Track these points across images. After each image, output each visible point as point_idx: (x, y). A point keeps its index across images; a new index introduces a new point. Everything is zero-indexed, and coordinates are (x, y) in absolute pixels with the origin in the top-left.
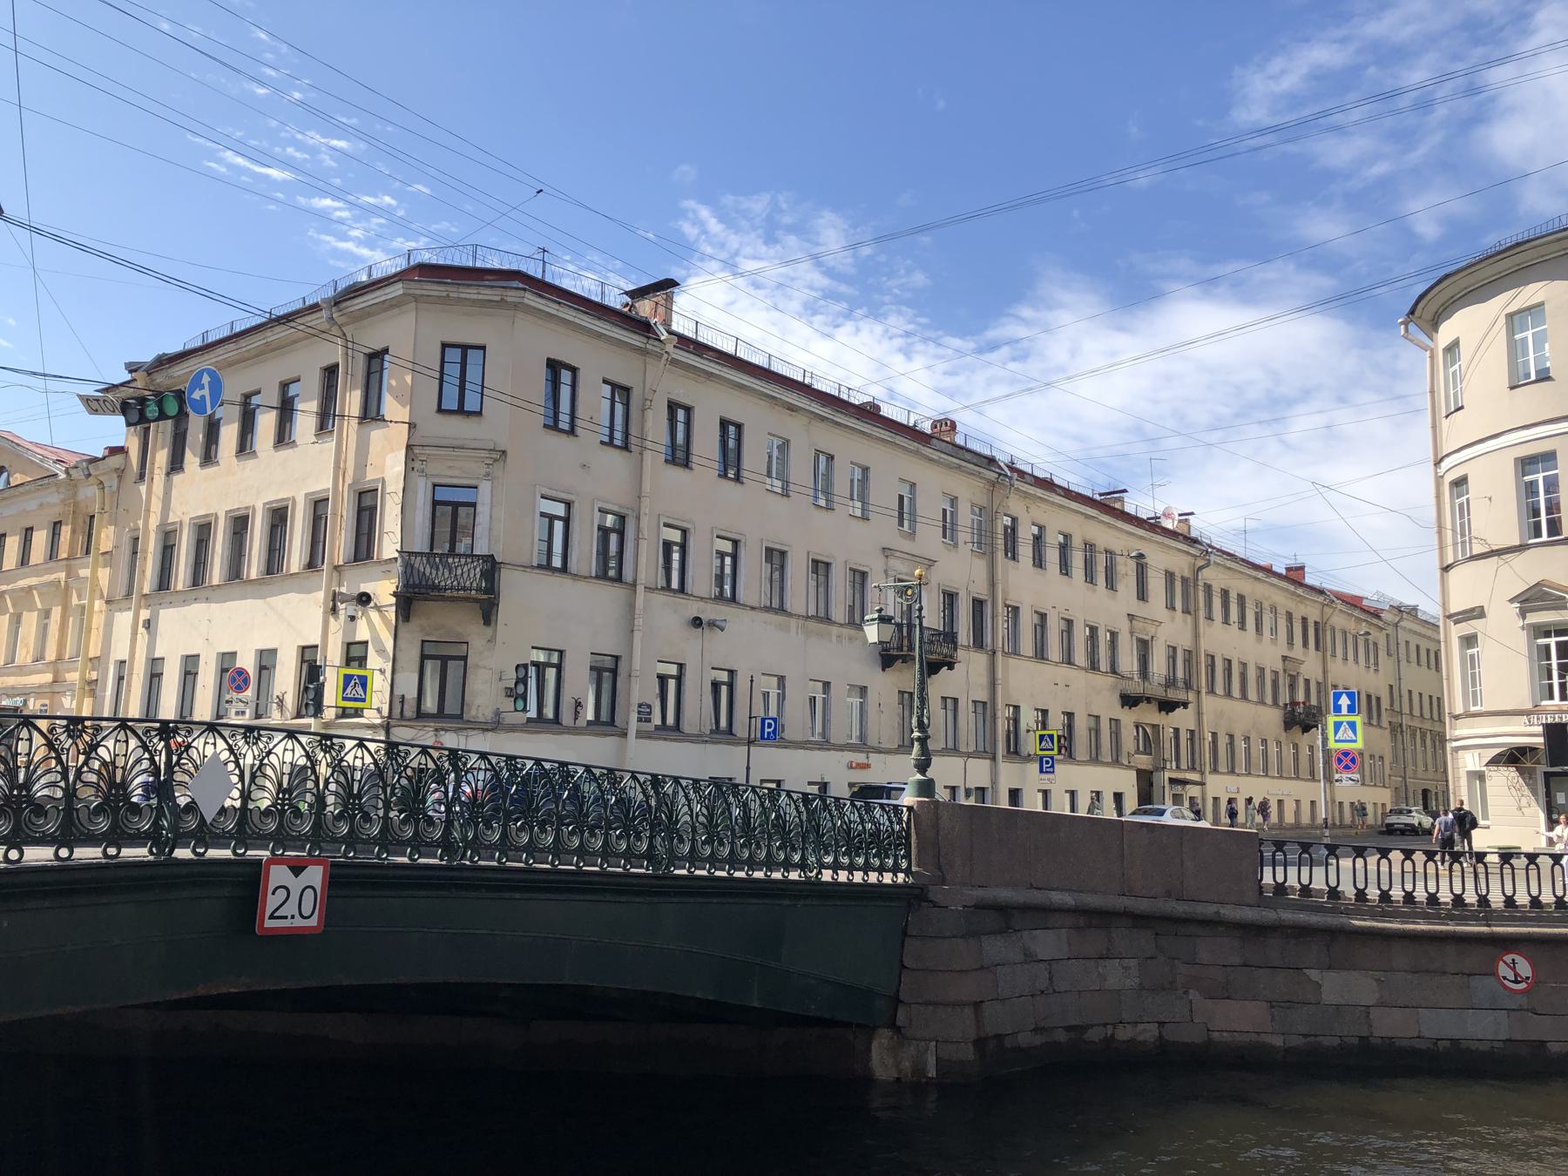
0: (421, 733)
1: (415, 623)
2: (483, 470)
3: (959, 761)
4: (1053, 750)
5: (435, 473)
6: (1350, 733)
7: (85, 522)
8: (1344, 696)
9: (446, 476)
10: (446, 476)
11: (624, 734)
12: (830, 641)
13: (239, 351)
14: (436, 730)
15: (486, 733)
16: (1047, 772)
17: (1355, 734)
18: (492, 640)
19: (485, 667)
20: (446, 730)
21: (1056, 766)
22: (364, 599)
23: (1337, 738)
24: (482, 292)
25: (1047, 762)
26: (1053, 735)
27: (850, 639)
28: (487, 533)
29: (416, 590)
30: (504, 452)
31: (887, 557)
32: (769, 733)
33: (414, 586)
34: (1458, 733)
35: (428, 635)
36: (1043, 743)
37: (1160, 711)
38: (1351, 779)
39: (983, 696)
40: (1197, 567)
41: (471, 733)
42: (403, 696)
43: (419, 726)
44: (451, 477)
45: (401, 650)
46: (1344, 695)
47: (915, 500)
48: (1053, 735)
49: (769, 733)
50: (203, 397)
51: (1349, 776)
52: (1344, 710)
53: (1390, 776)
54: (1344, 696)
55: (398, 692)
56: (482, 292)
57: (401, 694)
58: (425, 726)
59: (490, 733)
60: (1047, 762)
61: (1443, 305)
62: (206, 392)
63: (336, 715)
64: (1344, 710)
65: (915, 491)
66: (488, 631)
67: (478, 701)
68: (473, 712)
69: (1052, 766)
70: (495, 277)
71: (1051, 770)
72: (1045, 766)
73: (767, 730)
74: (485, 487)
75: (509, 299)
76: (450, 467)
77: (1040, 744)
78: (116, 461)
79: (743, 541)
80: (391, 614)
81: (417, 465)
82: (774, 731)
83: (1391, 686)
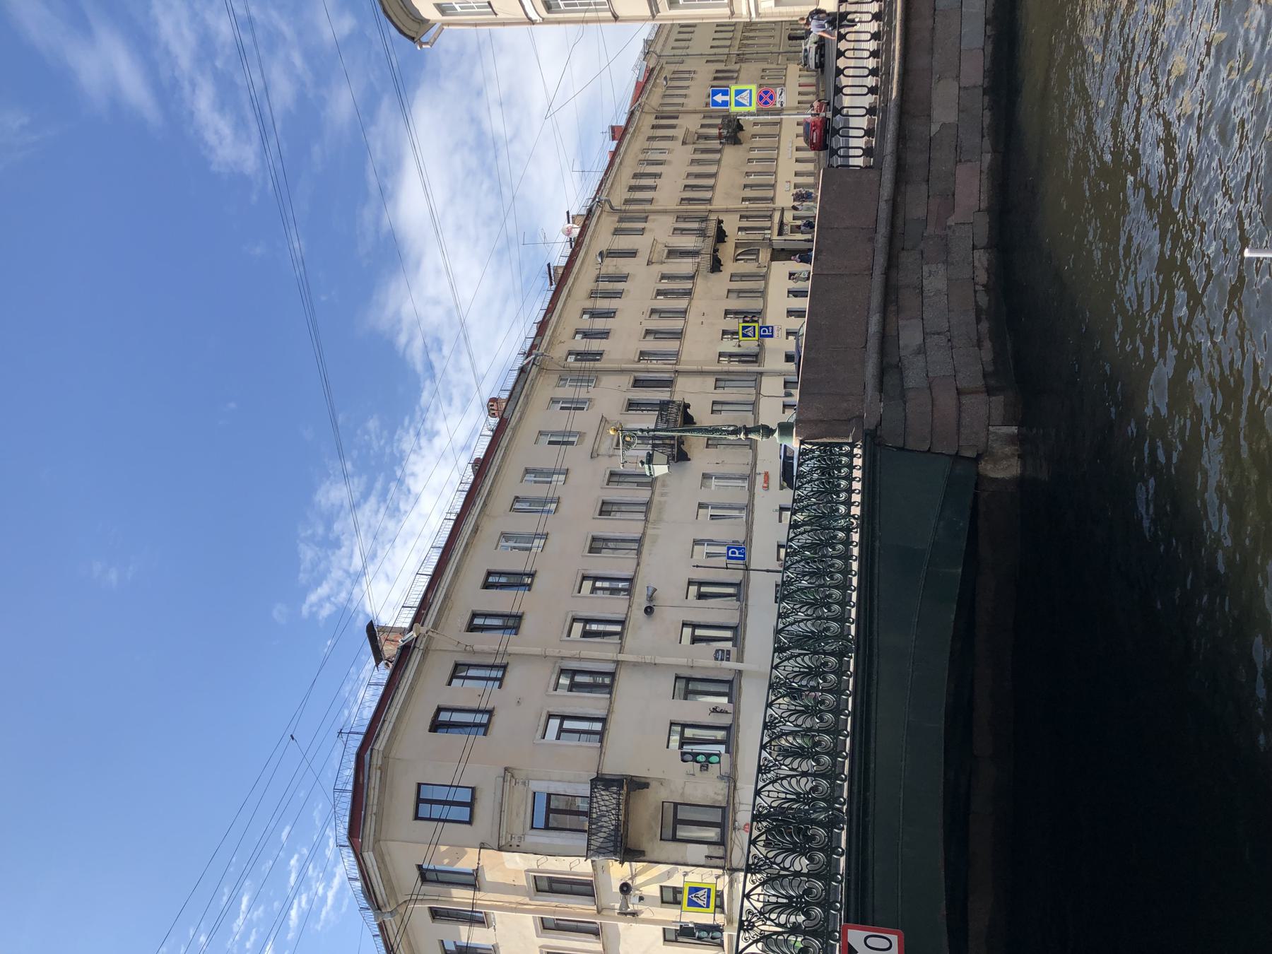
0: (737, 842)
1: (646, 846)
2: (520, 787)
4: (754, 327)
17: (746, 90)
18: (661, 782)
19: (683, 788)
20: (735, 821)
22: (625, 888)
24: (373, 786)
30: (506, 769)
31: (598, 455)
32: (740, 554)
34: (745, 12)
36: (749, 334)
38: (781, 95)
41: (737, 800)
42: (706, 857)
49: (740, 554)
52: (726, 98)
56: (373, 786)
58: (731, 839)
64: (726, 98)
65: (545, 432)
66: (653, 784)
67: (712, 794)
68: (720, 798)
69: (768, 327)
71: (770, 328)
72: (767, 333)
73: (737, 555)
74: (535, 786)
79: (583, 572)
81: (515, 842)
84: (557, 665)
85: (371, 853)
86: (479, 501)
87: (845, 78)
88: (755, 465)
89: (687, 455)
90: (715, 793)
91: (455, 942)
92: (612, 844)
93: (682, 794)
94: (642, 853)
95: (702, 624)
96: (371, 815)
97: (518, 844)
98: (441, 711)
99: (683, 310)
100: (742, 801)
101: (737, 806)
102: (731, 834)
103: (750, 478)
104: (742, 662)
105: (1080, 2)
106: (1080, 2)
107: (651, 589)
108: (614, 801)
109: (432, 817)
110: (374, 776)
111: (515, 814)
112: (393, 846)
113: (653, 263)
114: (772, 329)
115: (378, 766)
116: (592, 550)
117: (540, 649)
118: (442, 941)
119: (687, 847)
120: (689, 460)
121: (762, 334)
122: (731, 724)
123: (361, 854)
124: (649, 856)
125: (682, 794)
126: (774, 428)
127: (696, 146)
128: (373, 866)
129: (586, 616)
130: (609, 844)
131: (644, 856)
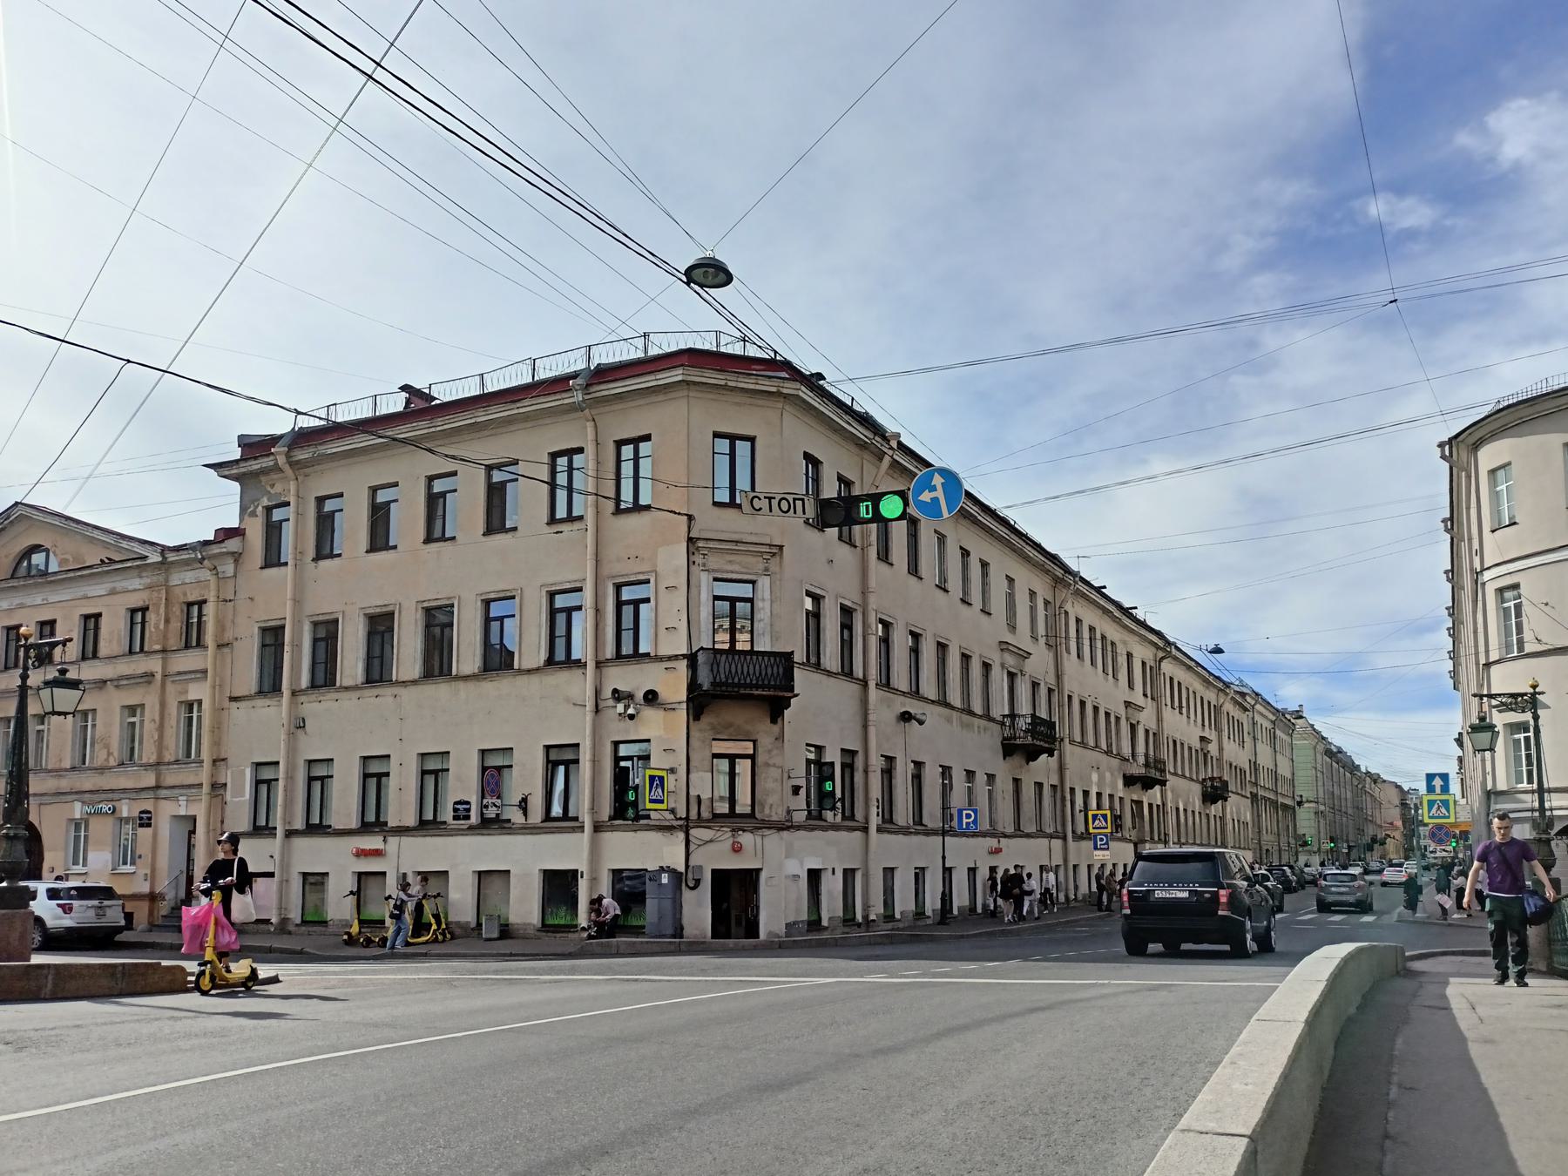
0: (720, 833)
1: (706, 720)
2: (761, 566)
3: (1045, 841)
4: (1107, 828)
5: (716, 567)
6: (1443, 810)
7: (182, 611)
8: (1437, 778)
9: (727, 572)
10: (727, 572)
11: (865, 829)
12: (974, 732)
13: (433, 430)
14: (733, 830)
15: (781, 832)
16: (1101, 849)
17: (1448, 812)
18: (780, 737)
19: (774, 765)
20: (744, 831)
21: (1111, 843)
22: (651, 697)
23: (1431, 814)
24: (760, 382)
25: (1101, 840)
26: (1106, 815)
27: (985, 730)
28: (769, 628)
29: (724, 688)
30: (781, 547)
31: (1002, 650)
32: (968, 824)
33: (721, 684)
34: (1555, 804)
35: (718, 733)
36: (1097, 822)
37: (1143, 789)
38: (1444, 850)
39: (1055, 780)
40: (1158, 659)
41: (767, 832)
42: (699, 796)
43: (718, 826)
44: (732, 572)
45: (694, 749)
46: (1437, 777)
47: (1014, 596)
48: (1106, 815)
49: (968, 824)
50: (936, 500)
51: (1443, 848)
52: (1438, 790)
53: (1252, 839)
54: (1437, 778)
55: (693, 793)
56: (760, 382)
57: (697, 794)
58: (722, 827)
59: (785, 832)
60: (1101, 840)
61: (1492, 431)
62: (940, 494)
63: (610, 817)
64: (1438, 790)
65: (1014, 587)
66: (776, 729)
67: (770, 800)
68: (767, 811)
69: (1107, 843)
70: (762, 367)
71: (1106, 846)
72: (1099, 843)
73: (965, 821)
74: (764, 583)
75: (785, 391)
76: (730, 562)
77: (1093, 824)
78: (233, 544)
79: (924, 635)
80: (682, 714)
81: (698, 559)
82: (975, 822)
83: (1250, 761)
84: (858, 608)
85: (680, 378)
86: (976, 509)
87: (688, 889)
88: (1005, 836)
89: (1009, 756)
90: (771, 805)
91: (396, 501)
92: (724, 680)
93: (767, 765)
94: (697, 718)
95: (893, 781)
96: (726, 379)
97: (696, 563)
98: (377, 490)
99: (1099, 743)
100: (766, 839)
101: (760, 832)
102: (728, 827)
103: (993, 833)
104: (877, 831)
105: (2, 1035)
106: (2, 1035)
107: (923, 718)
108: (736, 680)
109: (623, 463)
110: (771, 383)
111: (731, 559)
112: (681, 406)
113: (1126, 707)
114: (1104, 849)
115: (781, 389)
116: (939, 644)
117: (874, 586)
118: (398, 486)
119: (707, 771)
120: (1004, 759)
121: (1098, 837)
122: (826, 821)
123: (682, 365)
124: (694, 726)
125: (767, 765)
126: (1551, 873)
127: (1200, 751)
128: (657, 380)
129: (481, 646)
130: (723, 676)
131: (694, 720)
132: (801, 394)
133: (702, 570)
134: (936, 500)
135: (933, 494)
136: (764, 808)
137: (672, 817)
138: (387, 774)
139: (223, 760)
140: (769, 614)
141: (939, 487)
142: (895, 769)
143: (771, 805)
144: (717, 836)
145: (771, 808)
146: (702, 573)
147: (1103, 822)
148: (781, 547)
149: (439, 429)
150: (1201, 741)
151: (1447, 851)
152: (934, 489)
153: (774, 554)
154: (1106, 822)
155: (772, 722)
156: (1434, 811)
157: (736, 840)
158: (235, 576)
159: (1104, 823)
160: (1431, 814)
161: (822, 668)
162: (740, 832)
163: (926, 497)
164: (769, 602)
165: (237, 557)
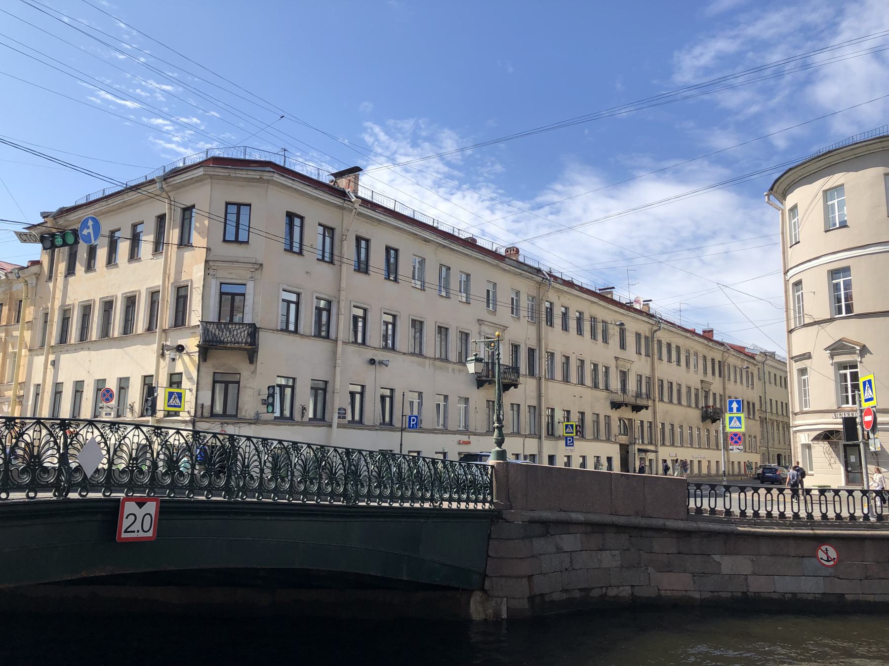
0: (214, 425)
4: (573, 433)
8: (735, 402)
9: (228, 278)
10: (228, 278)
12: (448, 372)
13: (108, 206)
15: (250, 425)
17: (741, 424)
19: (250, 388)
20: (228, 424)
22: (180, 349)
23: (731, 426)
24: (249, 173)
30: (261, 265)
32: (413, 424)
35: (217, 369)
36: (568, 429)
38: (738, 449)
41: (242, 425)
49: (413, 424)
50: (89, 233)
52: (735, 410)
53: (760, 447)
55: (200, 402)
60: (570, 440)
62: (91, 230)
63: (164, 415)
64: (735, 410)
66: (252, 367)
68: (243, 413)
69: (573, 442)
71: (572, 444)
72: (568, 442)
73: (412, 423)
74: (250, 285)
75: (265, 178)
78: (35, 269)
79: (399, 315)
85: (202, 173)
93: (246, 387)
96: (229, 172)
97: (210, 274)
100: (241, 429)
101: (238, 425)
113: (617, 361)
116: (414, 321)
120: (478, 388)
121: (568, 438)
124: (203, 365)
125: (246, 387)
126: (502, 447)
130: (210, 337)
132: (274, 179)
133: (213, 278)
134: (89, 233)
135: (88, 231)
136: (242, 411)
137: (188, 415)
138: (83, 391)
139: (259, 391)
140: (252, 302)
141: (91, 227)
142: (365, 392)
143: (246, 410)
144: (212, 427)
145: (246, 412)
146: (212, 279)
147: (571, 429)
148: (261, 265)
149: (111, 205)
150: (702, 383)
151: (739, 449)
152: (88, 228)
153: (257, 269)
154: (573, 430)
155: (250, 363)
156: (733, 423)
157: (223, 429)
158: (36, 285)
159: (572, 430)
160: (731, 426)
161: (298, 332)
162: (226, 425)
163: (85, 232)
164: (253, 296)
165: (38, 276)
